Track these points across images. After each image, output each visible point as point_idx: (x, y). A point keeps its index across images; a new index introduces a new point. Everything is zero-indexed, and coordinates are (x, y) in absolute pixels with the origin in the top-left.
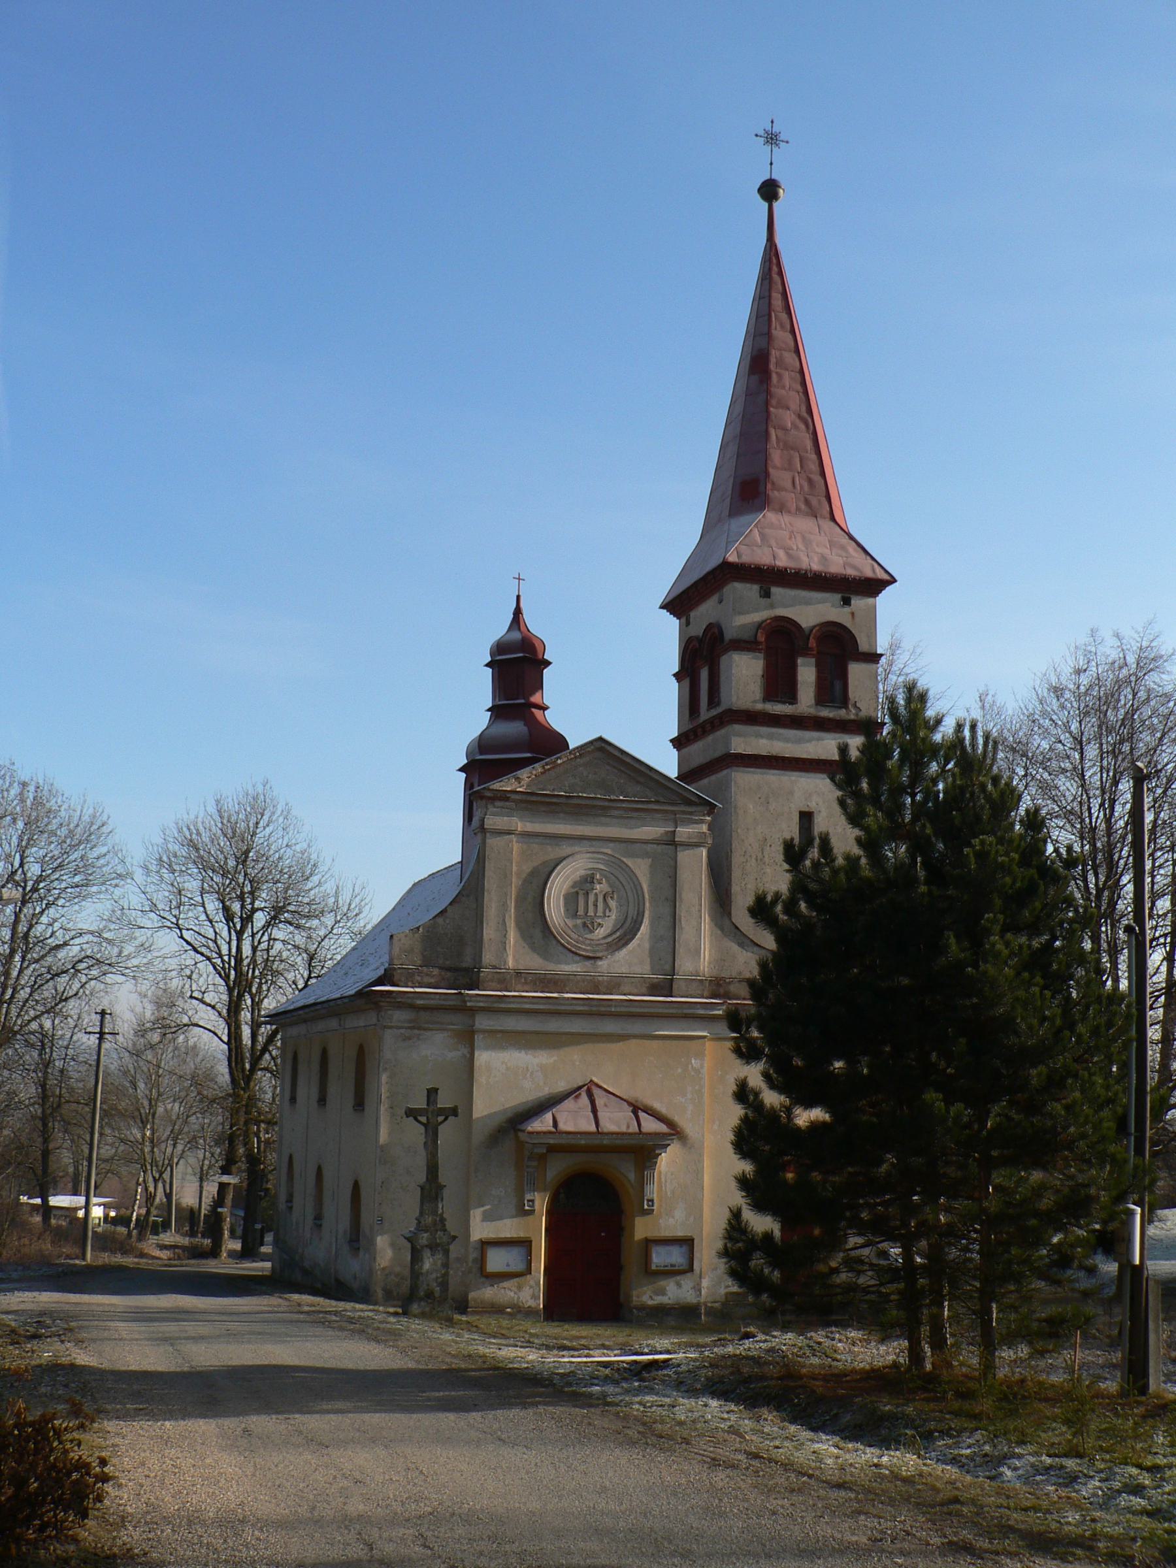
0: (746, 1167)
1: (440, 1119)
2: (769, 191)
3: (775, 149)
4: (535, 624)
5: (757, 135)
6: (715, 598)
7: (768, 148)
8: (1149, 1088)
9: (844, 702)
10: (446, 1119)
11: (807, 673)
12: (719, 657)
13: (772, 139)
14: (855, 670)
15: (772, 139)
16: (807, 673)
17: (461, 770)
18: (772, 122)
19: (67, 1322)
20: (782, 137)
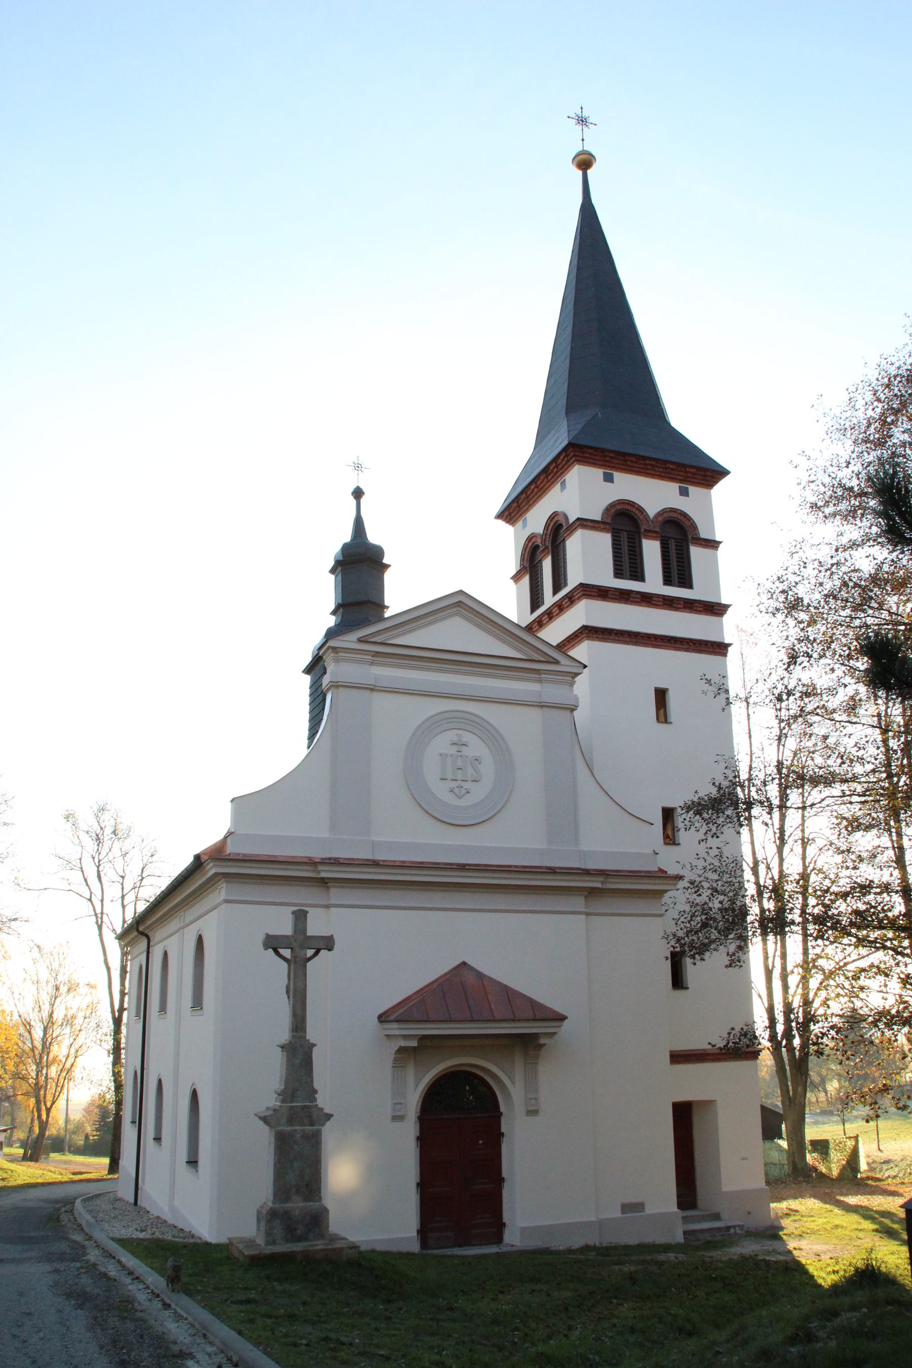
0: (316, 1096)
1: (310, 953)
2: (585, 162)
3: (585, 128)
4: (373, 537)
5: (569, 117)
6: (558, 486)
7: (579, 128)
8: (289, 1128)
9: (686, 581)
10: (317, 953)
11: (651, 550)
12: (564, 541)
13: (582, 121)
14: (696, 552)
15: (582, 121)
16: (651, 550)
17: (389, 566)
18: (582, 108)
19: (685, 468)
20: (590, 120)
